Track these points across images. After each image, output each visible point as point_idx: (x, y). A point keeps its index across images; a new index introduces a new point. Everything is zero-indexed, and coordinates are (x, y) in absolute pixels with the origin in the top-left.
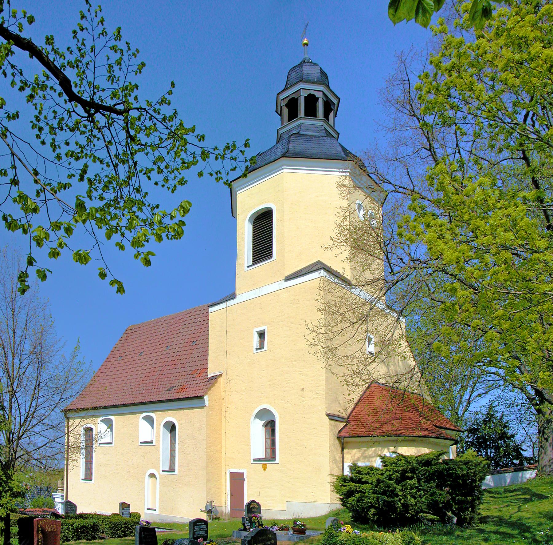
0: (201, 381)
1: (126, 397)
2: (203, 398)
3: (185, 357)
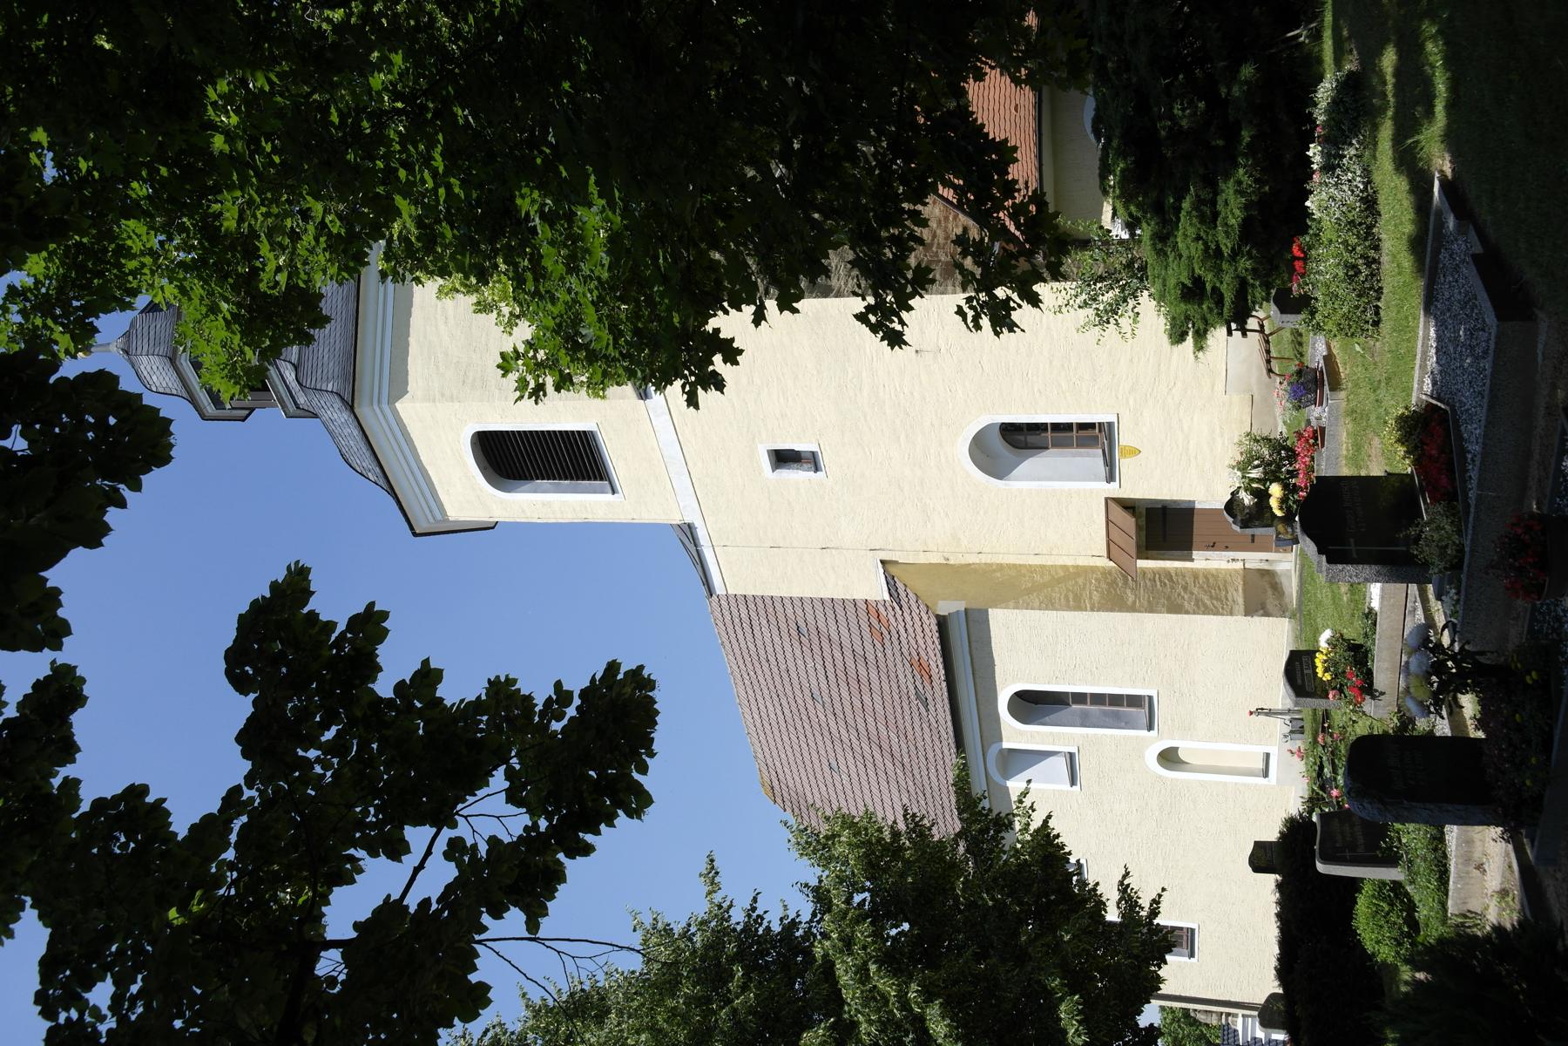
0: (900, 619)
1: (950, 819)
2: (944, 617)
3: (837, 654)
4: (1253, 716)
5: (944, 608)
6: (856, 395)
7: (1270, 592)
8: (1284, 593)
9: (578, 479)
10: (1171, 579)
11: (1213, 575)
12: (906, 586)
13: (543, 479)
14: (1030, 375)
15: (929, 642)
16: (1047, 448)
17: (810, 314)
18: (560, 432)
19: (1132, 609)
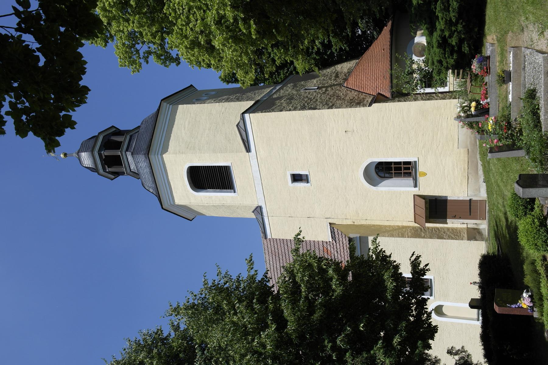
2: (352, 238)
4: (472, 285)
5: (352, 236)
6: (323, 150)
7: (477, 234)
8: (483, 234)
9: (222, 189)
10: (439, 230)
11: (455, 229)
12: (338, 229)
13: (210, 189)
14: (386, 141)
15: (345, 252)
16: (392, 178)
17: (309, 116)
18: (218, 166)
19: (424, 237)
